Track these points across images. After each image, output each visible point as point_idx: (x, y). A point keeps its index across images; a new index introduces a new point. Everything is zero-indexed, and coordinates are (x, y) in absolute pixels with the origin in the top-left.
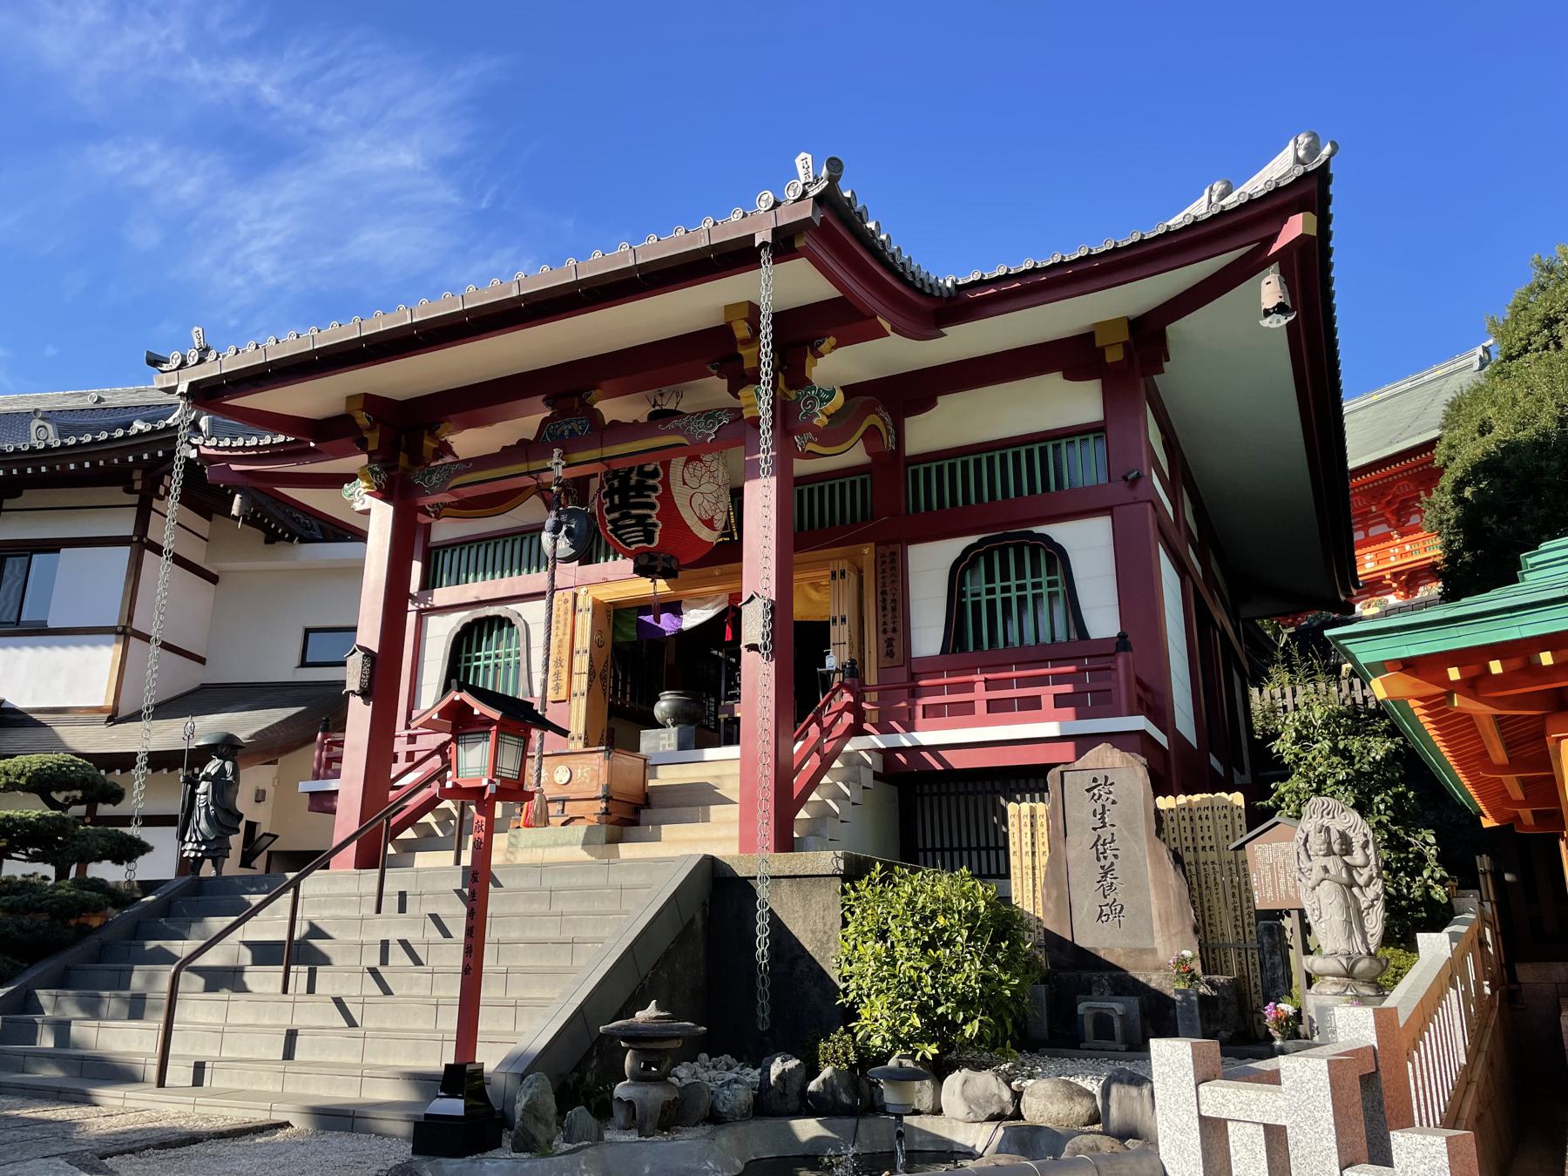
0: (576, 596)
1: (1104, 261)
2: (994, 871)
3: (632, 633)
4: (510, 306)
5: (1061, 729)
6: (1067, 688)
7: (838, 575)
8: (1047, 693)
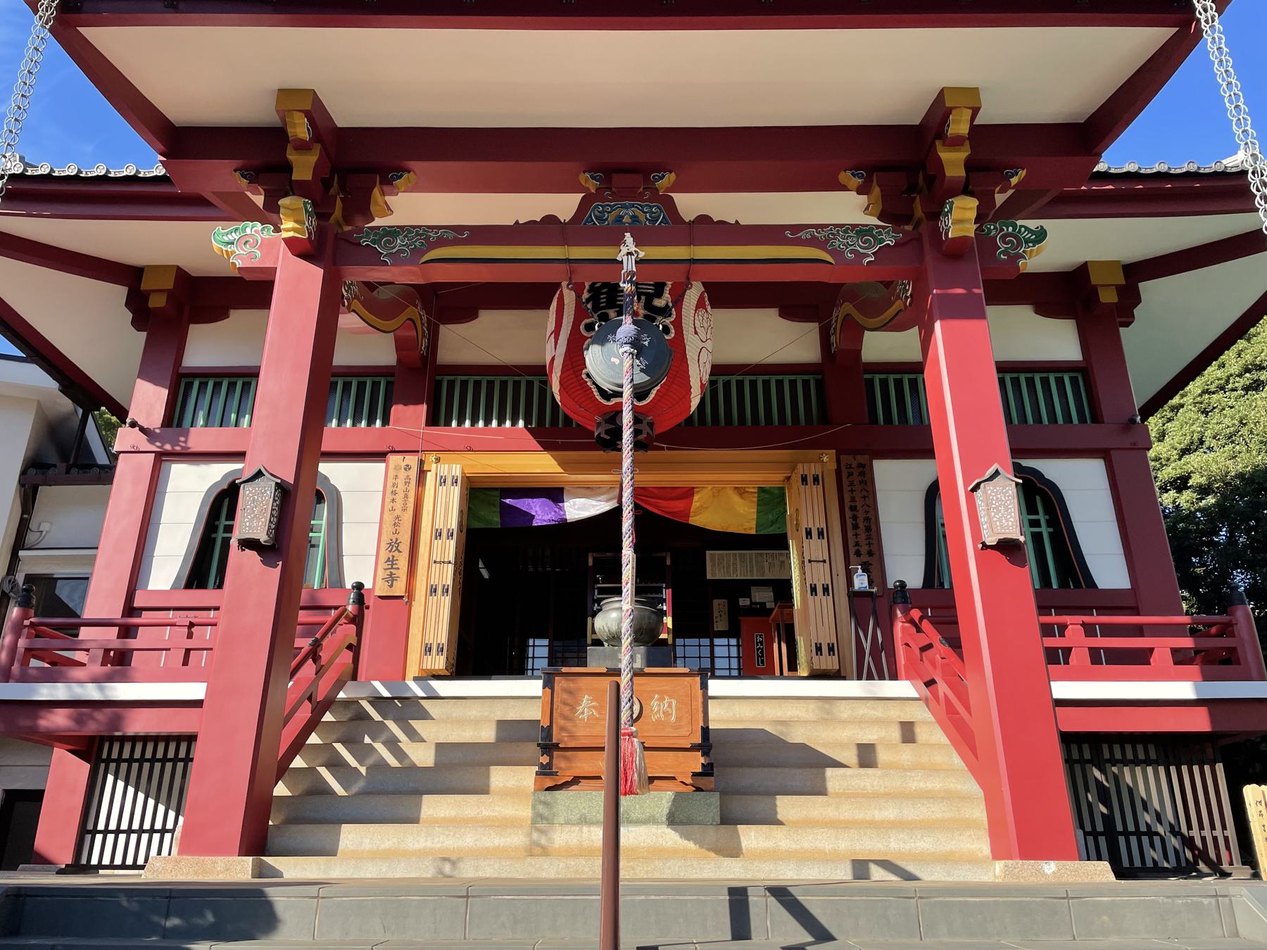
0: (422, 462)
1: (1150, 185)
2: (1137, 863)
3: (495, 520)
4: (646, 19)
5: (1197, 690)
6: (1187, 642)
7: (810, 479)
8: (1162, 647)
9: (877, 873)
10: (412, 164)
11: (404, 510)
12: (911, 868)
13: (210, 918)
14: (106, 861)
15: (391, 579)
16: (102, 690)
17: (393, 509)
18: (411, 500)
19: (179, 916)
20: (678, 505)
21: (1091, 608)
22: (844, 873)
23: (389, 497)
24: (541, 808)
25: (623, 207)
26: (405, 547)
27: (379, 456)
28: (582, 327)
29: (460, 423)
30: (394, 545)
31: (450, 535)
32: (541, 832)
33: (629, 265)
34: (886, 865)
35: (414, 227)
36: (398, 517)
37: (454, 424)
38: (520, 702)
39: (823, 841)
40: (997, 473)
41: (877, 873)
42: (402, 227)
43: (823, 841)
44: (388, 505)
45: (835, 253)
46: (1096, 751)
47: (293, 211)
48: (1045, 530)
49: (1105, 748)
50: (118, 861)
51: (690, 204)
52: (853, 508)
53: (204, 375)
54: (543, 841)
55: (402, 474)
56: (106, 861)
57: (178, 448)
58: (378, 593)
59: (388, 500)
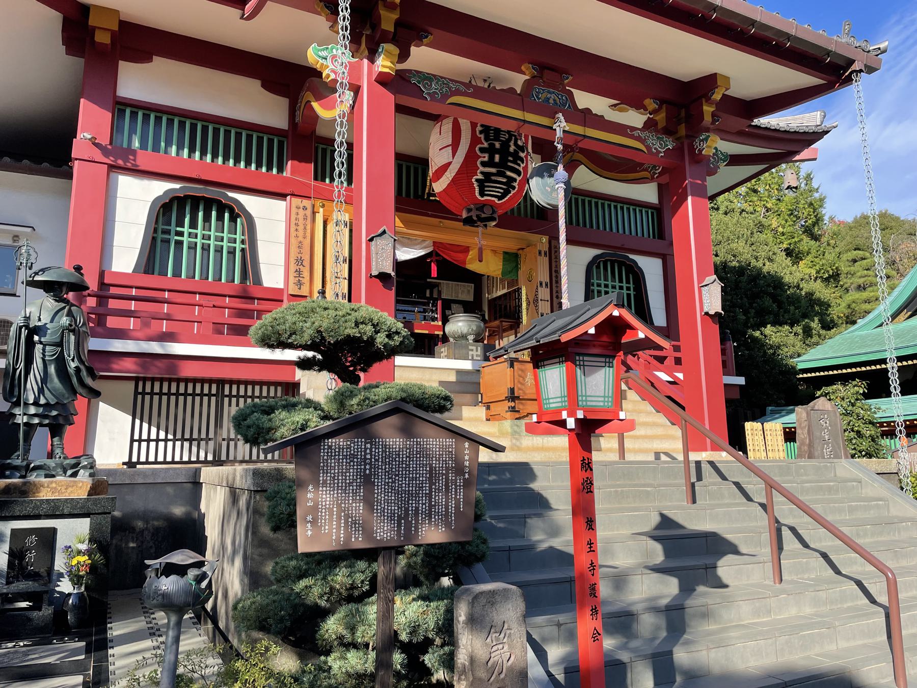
0: (314, 206)
9: (664, 458)
10: (431, 29)
12: (674, 455)
13: (508, 475)
14: (143, 459)
15: (300, 284)
16: (162, 347)
17: (297, 236)
18: (309, 231)
19: (495, 475)
20: (460, 256)
21: (254, 298)
22: (651, 458)
23: (293, 228)
24: (515, 428)
25: (550, 93)
26: (307, 263)
27: (282, 196)
28: (477, 149)
30: (299, 261)
32: (517, 439)
33: (559, 133)
34: (666, 454)
35: (442, 78)
38: (438, 371)
39: (647, 445)
40: (384, 232)
41: (664, 458)
42: (417, 72)
43: (647, 445)
44: (293, 233)
45: (648, 147)
47: (389, 54)
48: (632, 292)
49: (227, 387)
50: (161, 459)
51: (584, 99)
52: (297, 225)
53: (136, 106)
54: (518, 443)
55: (301, 212)
56: (143, 459)
57: (129, 165)
58: (291, 292)
59: (293, 230)
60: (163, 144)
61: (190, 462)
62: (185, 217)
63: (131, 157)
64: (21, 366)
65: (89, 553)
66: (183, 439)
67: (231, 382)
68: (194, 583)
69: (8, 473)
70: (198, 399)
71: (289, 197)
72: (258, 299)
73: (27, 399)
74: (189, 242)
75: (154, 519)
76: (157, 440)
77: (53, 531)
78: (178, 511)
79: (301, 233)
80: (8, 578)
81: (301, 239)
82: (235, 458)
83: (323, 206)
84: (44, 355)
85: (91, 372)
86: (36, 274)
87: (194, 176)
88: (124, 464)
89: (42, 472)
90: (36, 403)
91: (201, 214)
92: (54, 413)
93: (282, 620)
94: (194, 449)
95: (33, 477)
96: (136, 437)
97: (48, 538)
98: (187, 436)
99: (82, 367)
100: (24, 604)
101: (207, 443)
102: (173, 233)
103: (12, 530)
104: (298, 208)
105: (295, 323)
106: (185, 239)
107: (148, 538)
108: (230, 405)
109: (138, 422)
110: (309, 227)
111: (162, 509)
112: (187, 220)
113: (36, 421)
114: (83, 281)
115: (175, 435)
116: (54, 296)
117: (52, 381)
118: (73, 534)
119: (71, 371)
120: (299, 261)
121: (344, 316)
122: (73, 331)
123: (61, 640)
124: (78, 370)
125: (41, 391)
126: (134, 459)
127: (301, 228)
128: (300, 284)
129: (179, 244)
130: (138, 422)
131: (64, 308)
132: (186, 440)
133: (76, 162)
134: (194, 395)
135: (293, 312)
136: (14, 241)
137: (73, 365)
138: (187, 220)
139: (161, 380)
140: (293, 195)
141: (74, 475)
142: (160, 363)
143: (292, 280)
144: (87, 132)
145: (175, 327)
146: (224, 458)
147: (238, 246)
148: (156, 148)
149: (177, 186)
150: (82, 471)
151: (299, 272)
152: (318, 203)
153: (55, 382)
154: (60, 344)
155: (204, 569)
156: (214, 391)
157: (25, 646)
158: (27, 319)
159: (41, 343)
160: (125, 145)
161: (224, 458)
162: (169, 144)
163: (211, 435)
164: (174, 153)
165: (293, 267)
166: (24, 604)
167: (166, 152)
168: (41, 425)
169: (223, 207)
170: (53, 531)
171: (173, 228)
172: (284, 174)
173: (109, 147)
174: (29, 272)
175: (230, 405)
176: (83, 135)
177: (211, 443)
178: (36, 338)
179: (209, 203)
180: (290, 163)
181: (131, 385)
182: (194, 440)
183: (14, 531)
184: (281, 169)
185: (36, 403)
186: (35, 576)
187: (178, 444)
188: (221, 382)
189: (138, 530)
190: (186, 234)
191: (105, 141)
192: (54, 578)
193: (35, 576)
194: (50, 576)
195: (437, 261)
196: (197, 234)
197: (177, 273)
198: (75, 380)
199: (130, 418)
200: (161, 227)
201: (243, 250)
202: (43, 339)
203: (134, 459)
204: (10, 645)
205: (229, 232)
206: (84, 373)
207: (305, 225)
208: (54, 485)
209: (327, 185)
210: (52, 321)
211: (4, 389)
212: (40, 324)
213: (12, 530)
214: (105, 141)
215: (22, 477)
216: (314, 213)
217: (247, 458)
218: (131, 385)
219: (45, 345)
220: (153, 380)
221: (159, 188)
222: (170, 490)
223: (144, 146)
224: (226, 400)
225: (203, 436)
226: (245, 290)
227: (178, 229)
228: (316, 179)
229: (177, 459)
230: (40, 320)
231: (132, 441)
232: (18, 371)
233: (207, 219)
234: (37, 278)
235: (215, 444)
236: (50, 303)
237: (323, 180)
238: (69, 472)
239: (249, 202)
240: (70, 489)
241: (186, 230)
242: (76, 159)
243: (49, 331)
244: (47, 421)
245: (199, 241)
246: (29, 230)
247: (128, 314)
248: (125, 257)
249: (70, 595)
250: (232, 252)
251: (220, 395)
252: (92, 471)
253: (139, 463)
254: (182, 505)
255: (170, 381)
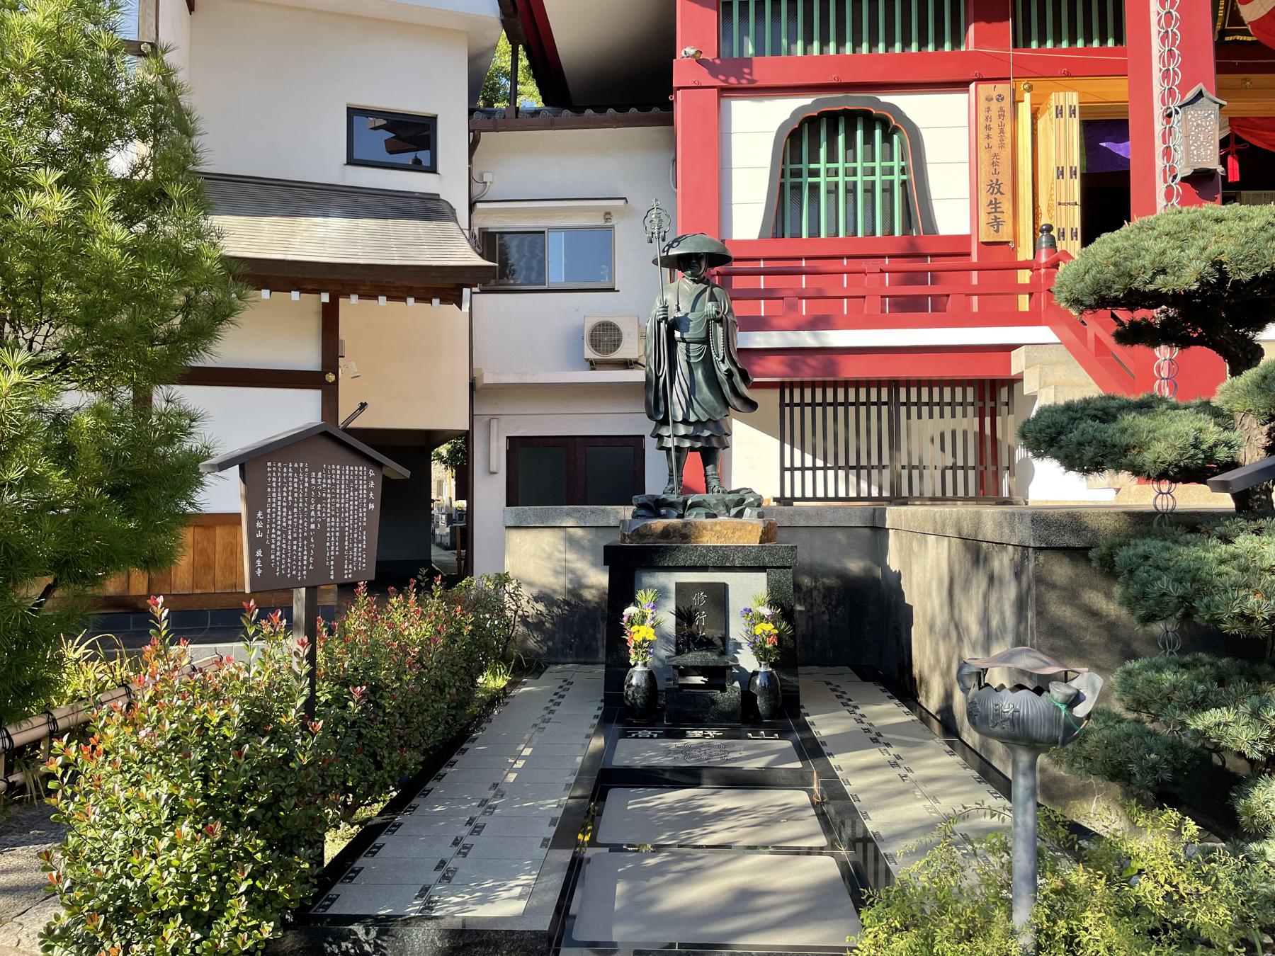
11: (1001, 147)
15: (996, 224)
16: (816, 337)
17: (989, 147)
18: (1008, 135)
21: (925, 256)
26: (1007, 189)
27: (960, 85)
29: (1042, 41)
30: (995, 187)
31: (1073, 173)
36: (995, 155)
37: (1034, 45)
40: (1200, 95)
46: (893, 393)
49: (903, 391)
55: (995, 106)
59: (982, 136)
60: (784, 42)
61: (826, 499)
62: (819, 147)
63: (746, 70)
64: (665, 368)
65: (773, 620)
66: (836, 468)
67: (908, 384)
68: (1063, 707)
69: (663, 511)
70: (808, 410)
71: (972, 86)
72: (933, 256)
73: (675, 416)
74: (828, 183)
75: (824, 575)
76: (814, 469)
77: (724, 587)
78: (855, 566)
79: (995, 141)
80: (677, 645)
81: (995, 150)
82: (921, 494)
83: (1030, 89)
84: (688, 357)
85: (745, 376)
86: (670, 246)
87: (831, 80)
88: (775, 500)
89: (702, 511)
90: (685, 421)
91: (841, 139)
92: (707, 433)
93: (1154, 768)
94: (853, 479)
95: (693, 517)
96: (787, 465)
97: (719, 596)
98: (853, 462)
99: (734, 370)
100: (698, 680)
101: (880, 472)
102: (805, 173)
103: (677, 584)
104: (989, 99)
105: (1163, 253)
106: (822, 180)
107: (819, 601)
108: (909, 417)
109: (787, 447)
110: (1008, 129)
111: (834, 563)
112: (823, 152)
113: (687, 444)
114: (725, 250)
115: (825, 460)
116: (692, 275)
117: (701, 390)
118: (748, 592)
119: (722, 376)
120: (995, 183)
121: (1262, 229)
122: (720, 321)
123: (770, 735)
124: (729, 374)
125: (689, 404)
126: (788, 494)
127: (995, 132)
128: (996, 224)
129: (814, 188)
130: (787, 447)
131: (705, 290)
132: (852, 468)
133: (679, 93)
134: (813, 405)
135: (1156, 233)
136: (607, 220)
137: (724, 367)
138: (823, 152)
139: (813, 385)
140: (981, 80)
141: (740, 514)
142: (812, 361)
143: (984, 218)
144: (689, 45)
145: (821, 308)
146: (905, 493)
147: (897, 178)
148: (776, 50)
149: (806, 101)
150: (748, 511)
151: (994, 205)
152: (1023, 85)
153: (704, 392)
154: (706, 341)
155: (1074, 684)
156: (884, 398)
157: (716, 737)
158: (665, 308)
159: (683, 340)
160: (736, 55)
161: (905, 493)
162: (792, 40)
163: (886, 461)
164: (800, 52)
165: (984, 198)
166: (698, 680)
167: (789, 52)
168: (692, 449)
169: (870, 120)
170: (724, 587)
171: (805, 166)
172: (963, 49)
173: (718, 61)
174: (663, 245)
175: (909, 417)
176: (685, 51)
177: (886, 473)
178: (677, 334)
179: (851, 117)
180: (972, 28)
181: (777, 392)
182: (863, 467)
183: (680, 587)
184: (956, 42)
185: (685, 421)
186: (706, 644)
187: (831, 473)
188: (894, 385)
189: (804, 589)
190: (823, 173)
191: (710, 55)
192: (730, 648)
193: (706, 644)
194: (723, 645)
195: (1238, 152)
196: (838, 168)
197: (814, 232)
198: (726, 388)
199: (778, 442)
200: (789, 166)
201: (904, 183)
202: (685, 336)
203: (788, 494)
204: (698, 733)
205: (883, 160)
206: (737, 378)
207: (1002, 126)
208: (718, 528)
209: (1035, 51)
210: (693, 310)
211: (647, 404)
212: (679, 315)
213: (677, 584)
214: (710, 55)
215: (681, 516)
216: (1015, 103)
217: (939, 494)
218: (777, 392)
219: (688, 343)
220: (802, 385)
221: (783, 109)
222: (840, 536)
223: (759, 51)
224: (903, 409)
225: (875, 462)
226: (912, 243)
227: (813, 166)
228: (1015, 46)
229: (820, 494)
230: (679, 310)
231: (783, 469)
232: (662, 380)
233: (850, 144)
234: (673, 252)
235: (892, 472)
236: (685, 283)
237: (1027, 44)
238: (734, 511)
239: (911, 105)
240: (738, 534)
241: (822, 165)
242: (679, 88)
243: (692, 324)
244: (699, 445)
245: (841, 179)
246: (622, 202)
247: (756, 295)
248: (747, 220)
249: (755, 673)
250: (888, 189)
251: (894, 403)
252: (759, 510)
253: (793, 499)
254: (860, 558)
255: (824, 385)
